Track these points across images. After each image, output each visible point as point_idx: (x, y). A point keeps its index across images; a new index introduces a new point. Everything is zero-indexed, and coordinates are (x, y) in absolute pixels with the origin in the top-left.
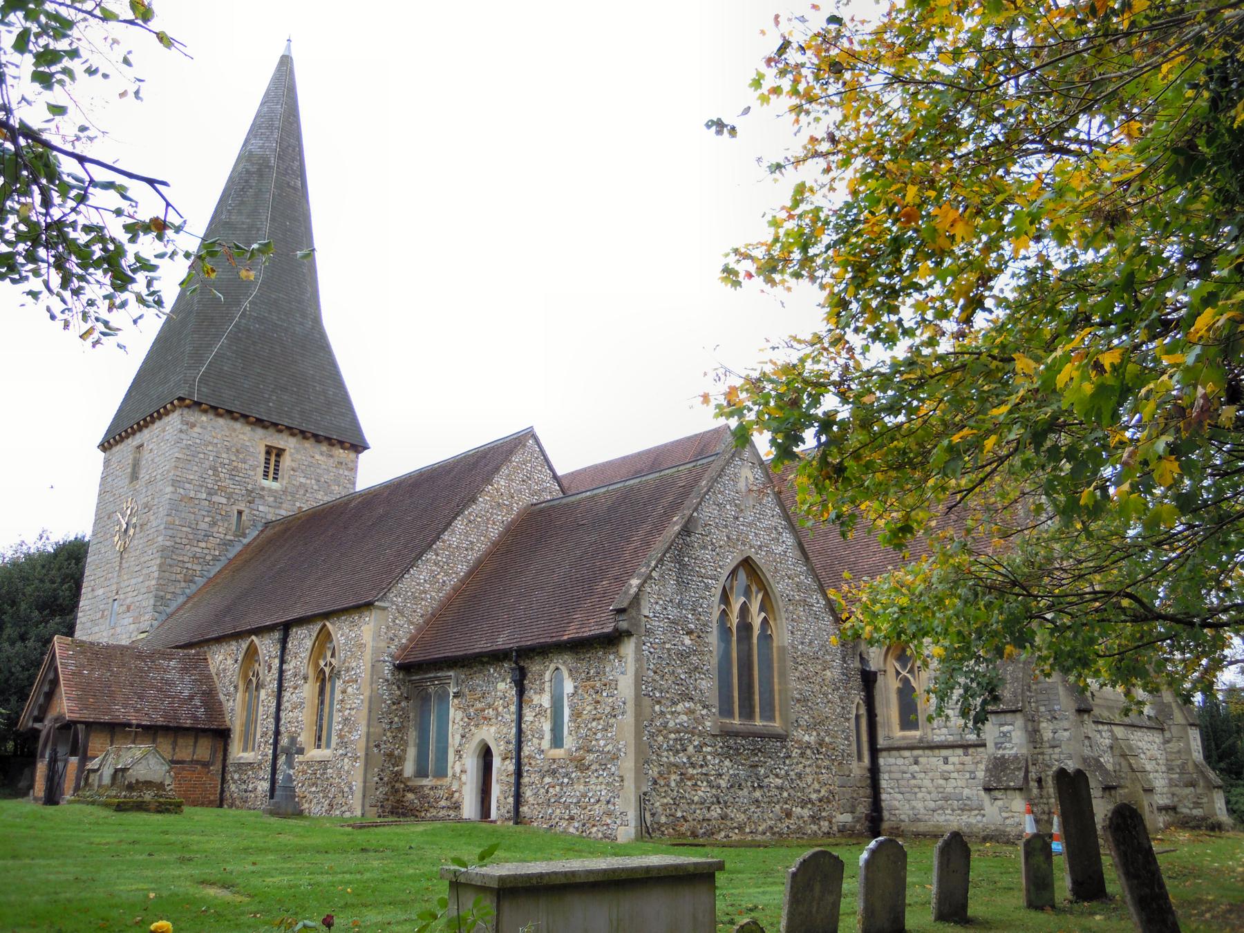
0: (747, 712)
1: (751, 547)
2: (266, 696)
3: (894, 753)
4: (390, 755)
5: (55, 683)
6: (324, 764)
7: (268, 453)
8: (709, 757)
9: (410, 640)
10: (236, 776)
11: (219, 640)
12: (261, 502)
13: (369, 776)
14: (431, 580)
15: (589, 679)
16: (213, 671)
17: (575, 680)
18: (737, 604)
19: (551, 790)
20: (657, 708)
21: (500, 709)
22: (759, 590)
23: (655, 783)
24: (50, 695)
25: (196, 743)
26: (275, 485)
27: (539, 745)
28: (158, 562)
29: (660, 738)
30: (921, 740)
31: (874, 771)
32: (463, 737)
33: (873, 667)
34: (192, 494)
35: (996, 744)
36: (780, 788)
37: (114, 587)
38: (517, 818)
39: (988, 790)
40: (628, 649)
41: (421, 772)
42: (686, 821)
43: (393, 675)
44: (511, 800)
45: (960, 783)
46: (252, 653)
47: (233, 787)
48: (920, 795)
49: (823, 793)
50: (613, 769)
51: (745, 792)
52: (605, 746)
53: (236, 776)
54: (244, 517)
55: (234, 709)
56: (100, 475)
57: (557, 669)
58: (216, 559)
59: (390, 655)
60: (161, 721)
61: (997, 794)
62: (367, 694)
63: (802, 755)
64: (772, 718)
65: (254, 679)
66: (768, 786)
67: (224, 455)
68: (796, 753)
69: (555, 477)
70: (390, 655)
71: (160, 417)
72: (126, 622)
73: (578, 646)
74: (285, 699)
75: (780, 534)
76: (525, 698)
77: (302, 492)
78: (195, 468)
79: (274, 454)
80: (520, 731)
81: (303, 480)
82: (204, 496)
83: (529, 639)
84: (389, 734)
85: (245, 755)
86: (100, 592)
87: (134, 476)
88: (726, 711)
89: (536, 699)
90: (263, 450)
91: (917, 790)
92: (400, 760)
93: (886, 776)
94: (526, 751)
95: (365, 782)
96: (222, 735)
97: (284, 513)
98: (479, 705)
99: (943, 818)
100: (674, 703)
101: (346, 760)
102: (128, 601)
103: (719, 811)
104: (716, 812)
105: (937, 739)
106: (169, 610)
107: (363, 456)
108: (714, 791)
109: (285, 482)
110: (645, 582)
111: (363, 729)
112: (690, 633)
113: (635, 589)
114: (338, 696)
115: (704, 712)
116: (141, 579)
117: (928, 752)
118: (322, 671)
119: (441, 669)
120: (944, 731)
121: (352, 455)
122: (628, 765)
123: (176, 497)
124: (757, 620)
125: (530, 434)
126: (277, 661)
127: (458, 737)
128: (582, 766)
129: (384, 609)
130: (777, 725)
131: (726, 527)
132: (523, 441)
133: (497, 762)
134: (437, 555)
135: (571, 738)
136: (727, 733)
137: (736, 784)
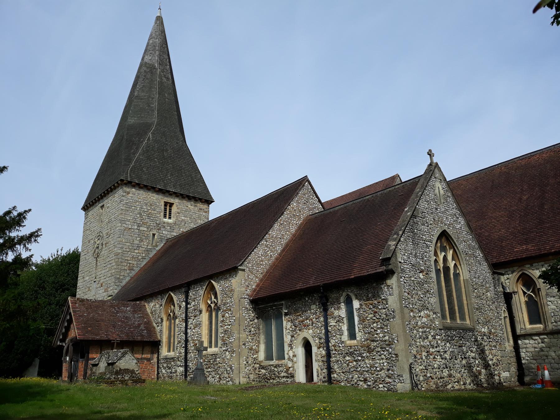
0: (453, 317)
1: (445, 225)
2: (179, 323)
5: (70, 322)
6: (215, 355)
7: (165, 205)
8: (439, 342)
9: (257, 286)
10: (165, 365)
13: (241, 361)
14: (265, 254)
16: (149, 311)
19: (350, 364)
20: (412, 314)
22: (450, 248)
23: (415, 357)
24: (68, 329)
25: (143, 350)
26: (170, 221)
31: (517, 348)
32: (292, 336)
34: (130, 227)
37: (94, 275)
38: (330, 380)
40: (393, 281)
42: (432, 379)
44: (325, 371)
46: (171, 301)
47: (164, 371)
49: (494, 361)
50: (390, 350)
54: (156, 237)
56: (83, 222)
57: (348, 295)
58: (143, 258)
59: (247, 295)
60: (125, 338)
65: (171, 314)
66: (469, 358)
67: (144, 207)
70: (247, 295)
71: (112, 191)
72: (101, 292)
75: (458, 218)
76: (329, 312)
77: (183, 224)
78: (131, 214)
80: (327, 331)
81: (183, 218)
82: (136, 227)
84: (249, 337)
85: (169, 354)
86: (87, 278)
88: (444, 317)
89: (336, 313)
90: (163, 204)
91: (545, 358)
94: (332, 342)
97: (175, 234)
102: (101, 282)
103: (447, 372)
104: (446, 373)
108: (443, 361)
109: (174, 219)
112: (422, 272)
113: (394, 247)
114: (220, 318)
115: (434, 316)
118: (210, 306)
123: (122, 228)
124: (451, 264)
127: (289, 337)
129: (244, 270)
131: (432, 213)
133: (314, 350)
134: (267, 242)
135: (360, 334)
136: (447, 328)
137: (453, 357)
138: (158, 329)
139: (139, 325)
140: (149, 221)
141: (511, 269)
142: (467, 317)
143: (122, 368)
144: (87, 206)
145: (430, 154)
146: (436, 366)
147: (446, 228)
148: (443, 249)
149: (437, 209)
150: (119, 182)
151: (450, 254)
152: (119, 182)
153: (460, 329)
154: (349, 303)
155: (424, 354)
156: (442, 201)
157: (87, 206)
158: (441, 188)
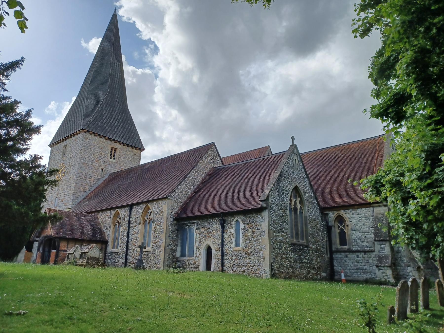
2: (123, 230)
3: (339, 253)
4: (172, 249)
7: (111, 150)
10: (110, 257)
11: (102, 211)
12: (109, 166)
14: (184, 191)
15: (250, 224)
16: (100, 221)
17: (244, 224)
18: (293, 202)
21: (215, 233)
23: (275, 259)
26: (114, 161)
27: (230, 246)
28: (74, 185)
29: (275, 244)
30: (348, 249)
31: (331, 260)
33: (330, 224)
34: (86, 162)
35: (379, 251)
36: (307, 263)
39: (377, 266)
40: (265, 214)
41: (183, 255)
43: (173, 222)
44: (220, 265)
45: (363, 264)
47: (109, 261)
48: (348, 268)
50: (260, 254)
51: (298, 264)
52: (257, 246)
53: (110, 257)
55: (109, 235)
57: (237, 220)
59: (172, 215)
61: (380, 268)
62: (165, 228)
63: (312, 252)
64: (303, 239)
65: (117, 224)
68: (311, 251)
69: (221, 159)
70: (172, 215)
72: (61, 205)
73: (246, 213)
74: (131, 230)
75: (305, 179)
77: (123, 163)
79: (113, 151)
80: (223, 242)
81: (123, 159)
82: (90, 163)
83: (227, 209)
85: (114, 250)
87: (64, 156)
88: (292, 237)
89: (229, 230)
90: (110, 149)
92: (175, 251)
93: (335, 261)
94: (225, 248)
95: (164, 258)
96: (105, 243)
98: (206, 232)
99: (356, 276)
100: (279, 233)
101: (156, 251)
102: (62, 198)
104: (290, 270)
105: (354, 249)
106: (78, 201)
107: (143, 153)
110: (270, 191)
111: (164, 240)
112: (282, 209)
114: (153, 229)
116: (67, 191)
117: (351, 253)
119: (191, 220)
120: (357, 246)
121: (139, 152)
122: (266, 253)
123: (81, 163)
124: (299, 206)
126: (128, 218)
127: (198, 243)
128: (247, 253)
129: (171, 199)
130: (304, 242)
132: (211, 147)
133: (213, 252)
136: (293, 244)
137: (295, 261)
138: (106, 233)
139: (94, 230)
140: (97, 158)
141: (333, 212)
142: (305, 238)
143: (92, 256)
144: (53, 144)
145: (293, 138)
146: (285, 265)
147: (297, 184)
148: (296, 197)
149: (293, 173)
150: (81, 130)
151: (298, 200)
152: (81, 130)
153: (300, 245)
155: (280, 258)
156: (297, 168)
157: (53, 144)
158: (297, 160)
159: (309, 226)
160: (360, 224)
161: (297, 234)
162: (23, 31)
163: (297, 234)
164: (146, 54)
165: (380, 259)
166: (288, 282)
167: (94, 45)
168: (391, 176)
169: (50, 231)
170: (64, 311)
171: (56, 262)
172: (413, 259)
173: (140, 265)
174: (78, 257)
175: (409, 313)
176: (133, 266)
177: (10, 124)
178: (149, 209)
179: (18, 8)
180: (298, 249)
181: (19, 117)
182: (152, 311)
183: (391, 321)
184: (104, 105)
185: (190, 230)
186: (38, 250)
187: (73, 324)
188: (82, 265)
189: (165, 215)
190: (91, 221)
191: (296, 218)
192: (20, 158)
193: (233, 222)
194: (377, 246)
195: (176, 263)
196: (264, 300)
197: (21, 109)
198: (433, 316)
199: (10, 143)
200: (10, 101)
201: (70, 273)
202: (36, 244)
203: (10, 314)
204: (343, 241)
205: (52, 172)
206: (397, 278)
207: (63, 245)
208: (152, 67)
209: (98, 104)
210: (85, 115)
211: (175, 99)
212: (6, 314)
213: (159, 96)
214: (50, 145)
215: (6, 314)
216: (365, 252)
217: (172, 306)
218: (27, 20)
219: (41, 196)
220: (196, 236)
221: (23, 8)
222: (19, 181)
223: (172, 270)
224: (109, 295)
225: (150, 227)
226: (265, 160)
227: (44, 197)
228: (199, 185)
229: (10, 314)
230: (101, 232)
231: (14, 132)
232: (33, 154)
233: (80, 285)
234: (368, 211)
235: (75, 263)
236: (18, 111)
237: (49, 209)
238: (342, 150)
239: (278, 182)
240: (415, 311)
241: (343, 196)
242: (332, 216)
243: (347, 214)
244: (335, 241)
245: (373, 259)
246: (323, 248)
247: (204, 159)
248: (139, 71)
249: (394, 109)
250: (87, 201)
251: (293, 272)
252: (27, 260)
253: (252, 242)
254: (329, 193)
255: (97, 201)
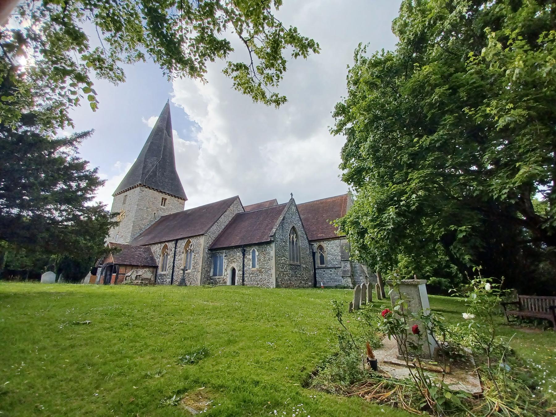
2: (170, 258)
14: (216, 229)
16: (153, 252)
26: (164, 207)
27: (249, 267)
31: (315, 273)
40: (273, 245)
41: (215, 274)
44: (241, 281)
46: (166, 247)
55: (159, 261)
73: (260, 244)
79: (164, 200)
80: (243, 264)
87: (124, 203)
88: (290, 260)
89: (248, 257)
92: (210, 272)
94: (245, 269)
96: (156, 267)
111: (201, 264)
114: (193, 257)
122: (273, 271)
125: (237, 197)
127: (226, 266)
130: (298, 263)
132: (236, 199)
133: (237, 272)
138: (157, 260)
139: (147, 258)
145: (292, 194)
154: (254, 252)
159: (301, 252)
160: (332, 250)
161: (294, 258)
162: (94, 111)
163: (294, 258)
164: (192, 131)
165: (344, 272)
166: (287, 290)
167: (153, 122)
168: (351, 219)
169: (111, 259)
170: (122, 320)
171: (116, 283)
172: (363, 271)
173: (183, 283)
174: (134, 278)
175: (360, 305)
176: (177, 283)
177: (80, 178)
178: (190, 242)
179: (91, 94)
180: (295, 268)
181: (88, 173)
182: (191, 316)
183: (351, 311)
184: (157, 168)
185: (220, 257)
186: (102, 274)
187: (129, 329)
188: (137, 285)
189: (202, 247)
190: (145, 252)
191: (293, 247)
192: (87, 204)
193: (251, 251)
194: (343, 264)
195: (210, 280)
196: (271, 303)
197: (89, 167)
198: (374, 306)
199: (80, 193)
200: (81, 161)
201: (127, 290)
202: (99, 270)
203: (78, 324)
204: (322, 262)
205: (114, 215)
206: (354, 283)
207: (122, 270)
208: (196, 141)
209: (153, 166)
210: (143, 174)
211: (214, 164)
212: (74, 324)
213: (201, 161)
214: (113, 195)
215: (74, 324)
216: (335, 268)
217: (207, 311)
218: (98, 102)
219: (105, 233)
220: (225, 261)
221: (96, 94)
222: (86, 222)
223: (207, 286)
224: (158, 306)
225: (191, 256)
226: (273, 209)
227: (107, 234)
228: (227, 226)
229: (78, 324)
230: (152, 259)
231: (83, 184)
232: (98, 201)
233: (135, 300)
234: (337, 242)
235: (131, 283)
236: (87, 168)
237: (111, 243)
238: (322, 203)
239: (282, 223)
240: (364, 304)
241: (322, 233)
242: (316, 245)
243: (324, 244)
244: (317, 260)
245: (340, 272)
246: (311, 267)
247: (231, 207)
248: (188, 143)
249: (355, 177)
250: (143, 236)
251: (290, 283)
252: (92, 281)
253: (264, 264)
254: (313, 231)
255: (150, 237)
